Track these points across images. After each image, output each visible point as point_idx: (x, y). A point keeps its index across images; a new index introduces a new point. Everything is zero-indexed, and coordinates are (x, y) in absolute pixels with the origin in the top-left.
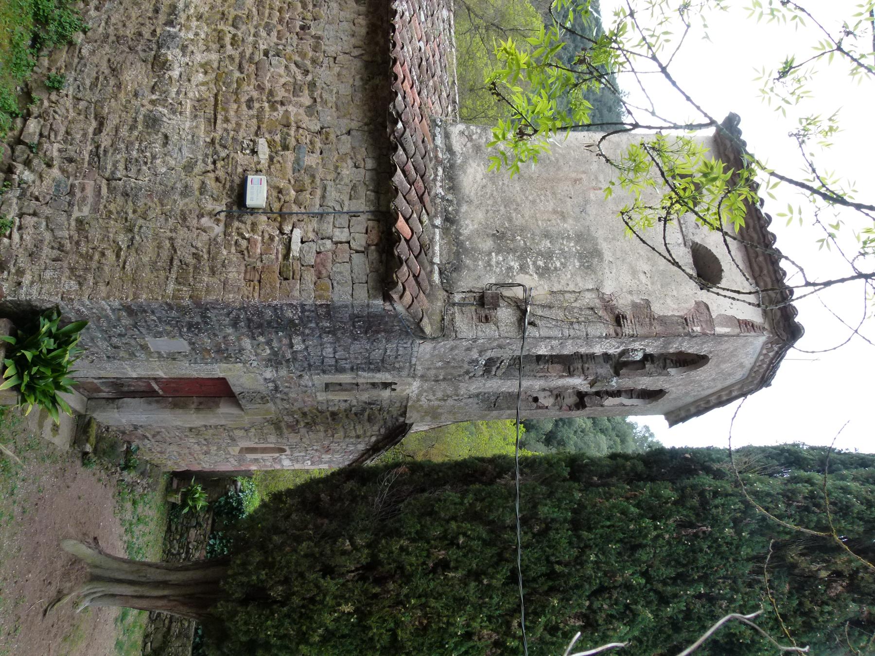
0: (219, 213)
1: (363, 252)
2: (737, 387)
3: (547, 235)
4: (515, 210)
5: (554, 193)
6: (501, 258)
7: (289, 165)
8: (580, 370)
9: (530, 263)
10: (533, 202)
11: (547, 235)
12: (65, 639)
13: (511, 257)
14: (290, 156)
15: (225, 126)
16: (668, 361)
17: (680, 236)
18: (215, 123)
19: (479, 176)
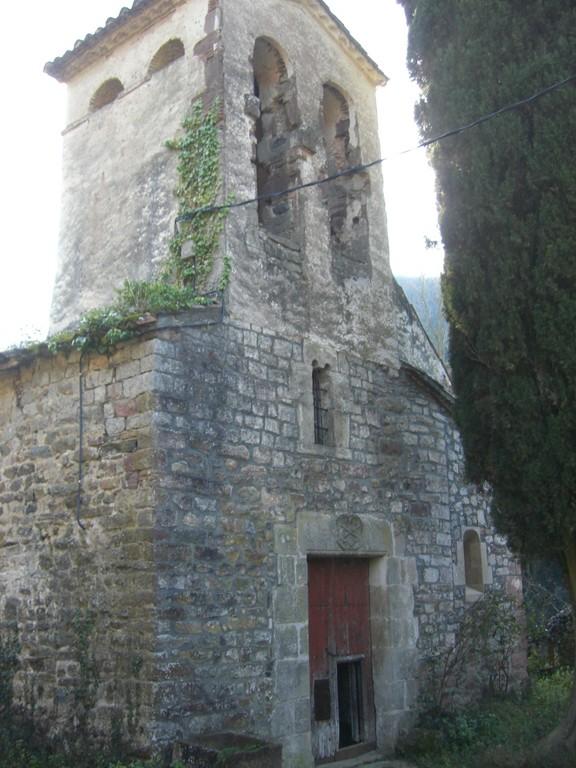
0: (81, 526)
1: (115, 370)
2: (315, 13)
3: (139, 213)
4: (118, 250)
5: (106, 217)
6: (157, 252)
7: (44, 461)
8: (292, 165)
9: (161, 221)
10: (112, 234)
11: (139, 213)
12: (139, 471)
13: (155, 243)
14: (39, 463)
15: (14, 533)
16: (282, 80)
17: (141, 88)
18: (12, 544)
19: (90, 294)
